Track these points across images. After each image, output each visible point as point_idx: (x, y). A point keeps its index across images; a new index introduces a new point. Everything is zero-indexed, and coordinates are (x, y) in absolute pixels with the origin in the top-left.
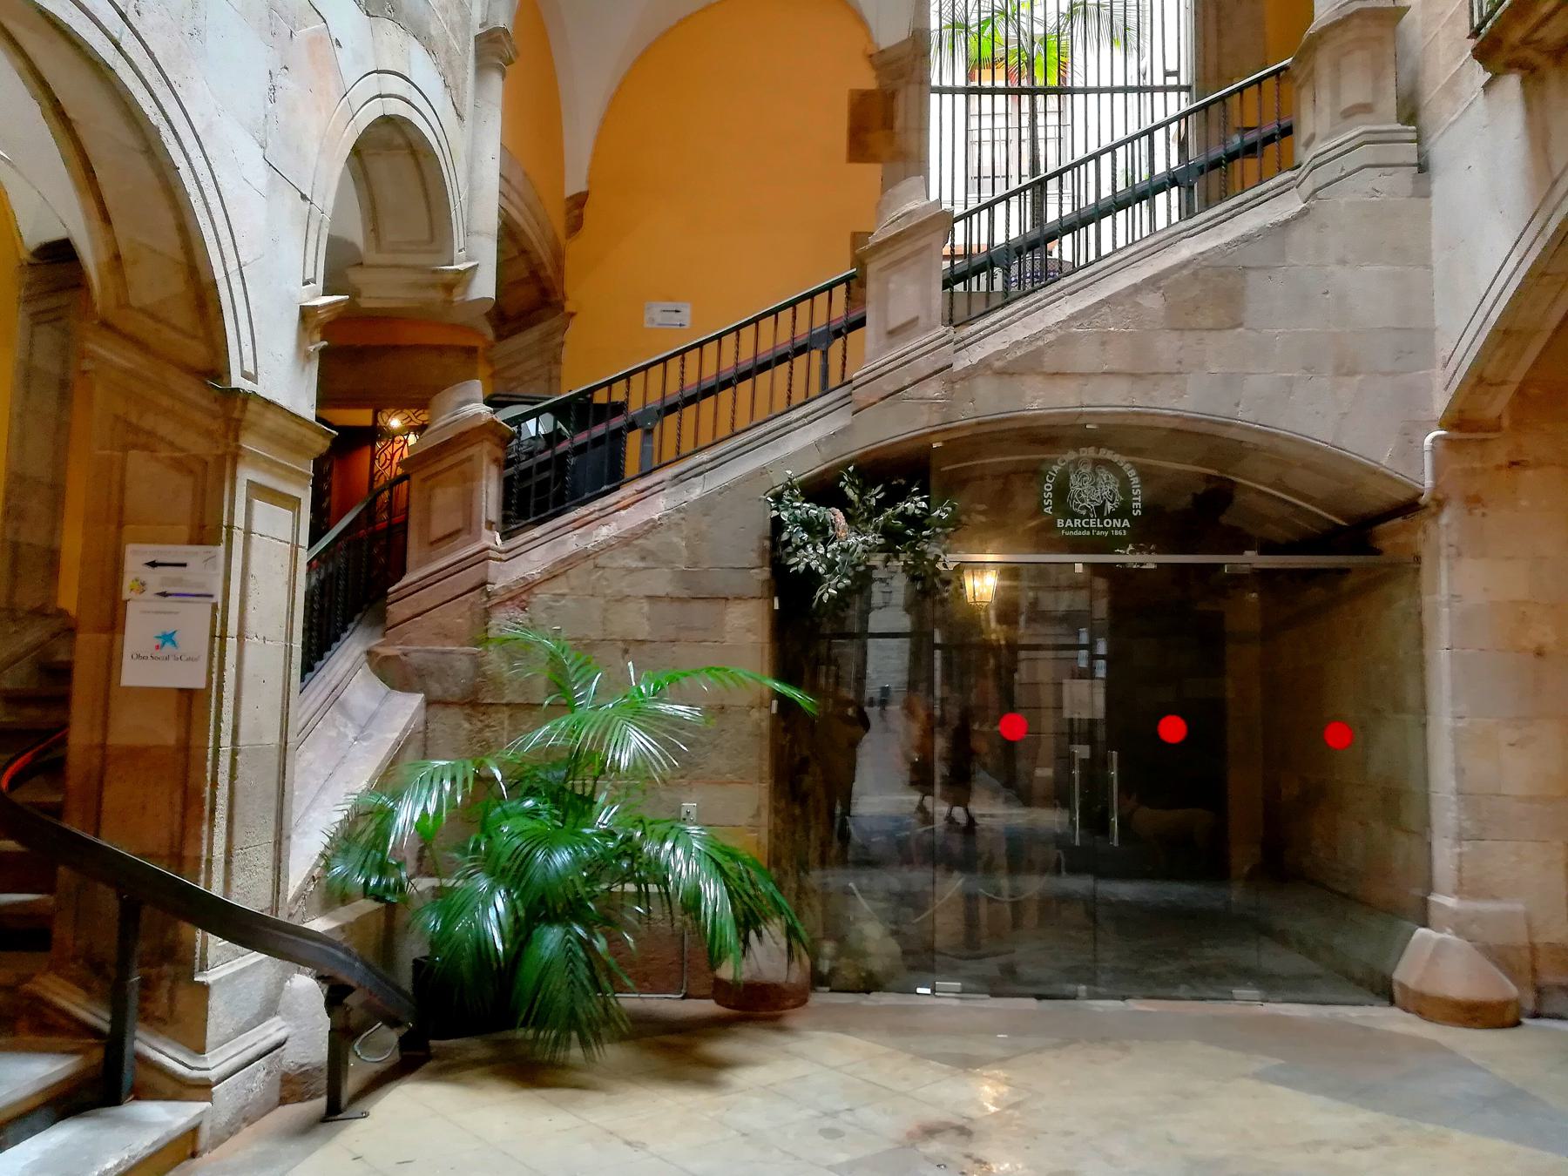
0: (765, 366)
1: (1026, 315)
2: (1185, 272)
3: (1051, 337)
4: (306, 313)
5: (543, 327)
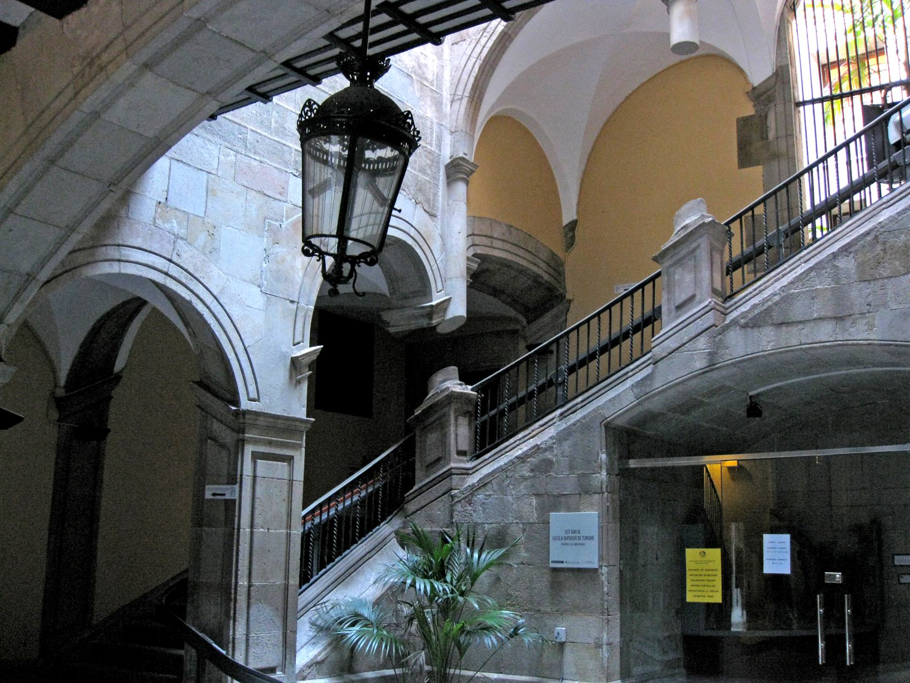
0: (626, 336)
1: (776, 281)
2: (868, 238)
3: (777, 298)
4: (295, 363)
5: (554, 311)
